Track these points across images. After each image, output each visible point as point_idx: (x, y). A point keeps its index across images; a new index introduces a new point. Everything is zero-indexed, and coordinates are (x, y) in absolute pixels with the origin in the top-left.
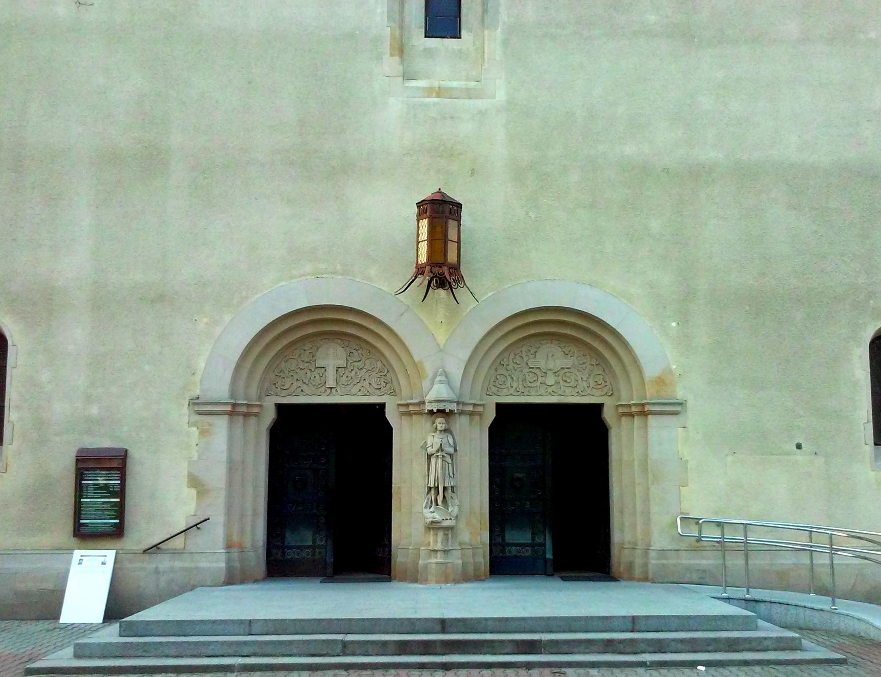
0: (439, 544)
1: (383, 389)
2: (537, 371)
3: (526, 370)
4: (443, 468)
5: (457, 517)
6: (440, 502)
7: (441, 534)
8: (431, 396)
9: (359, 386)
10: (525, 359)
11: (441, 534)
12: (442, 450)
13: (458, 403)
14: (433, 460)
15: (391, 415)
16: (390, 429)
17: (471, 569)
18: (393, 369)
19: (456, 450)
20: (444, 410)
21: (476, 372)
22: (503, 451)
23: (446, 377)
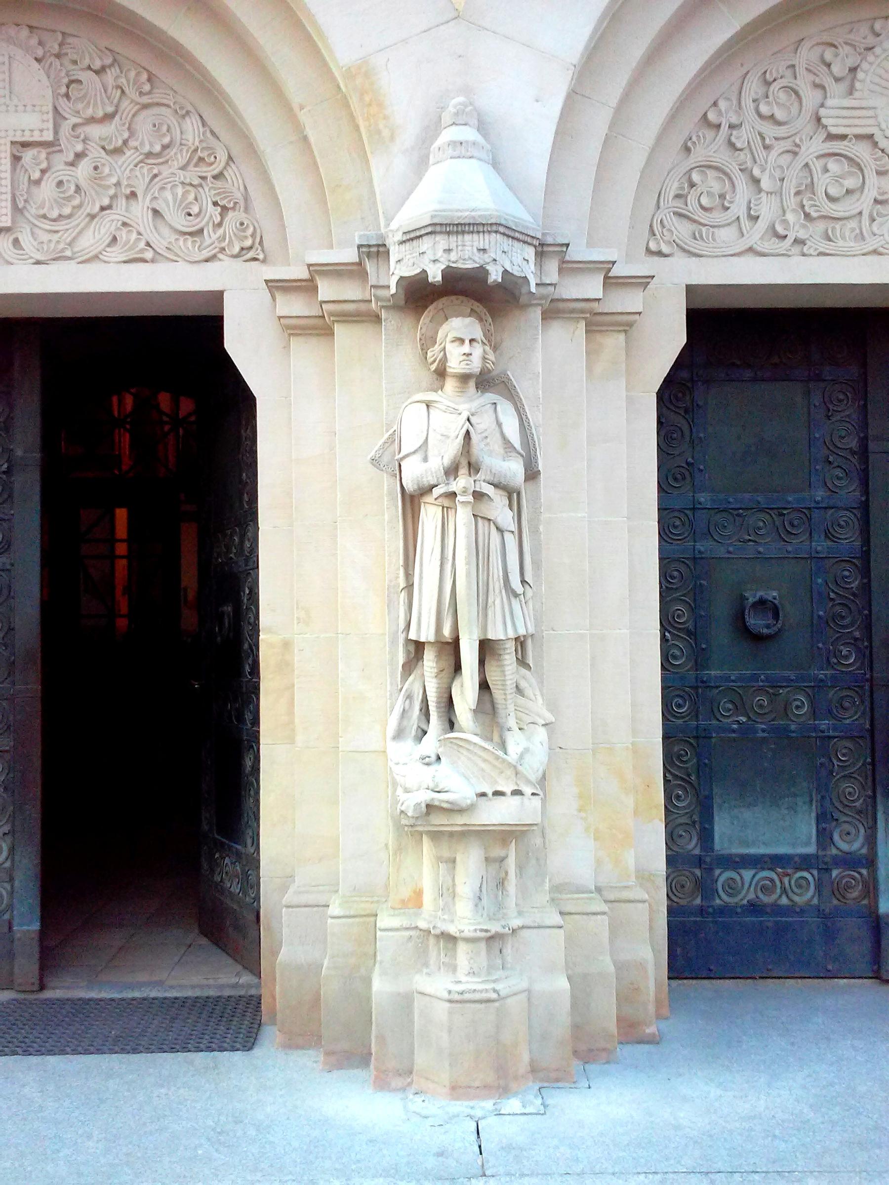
1: (211, 236)
2: (862, 151)
3: (815, 146)
7: (470, 864)
8: (418, 209)
9: (107, 225)
10: (811, 98)
11: (470, 864)
12: (473, 468)
13: (542, 250)
14: (430, 515)
15: (247, 346)
17: (605, 1010)
18: (251, 149)
19: (532, 474)
20: (482, 272)
21: (603, 164)
22: (703, 498)
23: (482, 127)
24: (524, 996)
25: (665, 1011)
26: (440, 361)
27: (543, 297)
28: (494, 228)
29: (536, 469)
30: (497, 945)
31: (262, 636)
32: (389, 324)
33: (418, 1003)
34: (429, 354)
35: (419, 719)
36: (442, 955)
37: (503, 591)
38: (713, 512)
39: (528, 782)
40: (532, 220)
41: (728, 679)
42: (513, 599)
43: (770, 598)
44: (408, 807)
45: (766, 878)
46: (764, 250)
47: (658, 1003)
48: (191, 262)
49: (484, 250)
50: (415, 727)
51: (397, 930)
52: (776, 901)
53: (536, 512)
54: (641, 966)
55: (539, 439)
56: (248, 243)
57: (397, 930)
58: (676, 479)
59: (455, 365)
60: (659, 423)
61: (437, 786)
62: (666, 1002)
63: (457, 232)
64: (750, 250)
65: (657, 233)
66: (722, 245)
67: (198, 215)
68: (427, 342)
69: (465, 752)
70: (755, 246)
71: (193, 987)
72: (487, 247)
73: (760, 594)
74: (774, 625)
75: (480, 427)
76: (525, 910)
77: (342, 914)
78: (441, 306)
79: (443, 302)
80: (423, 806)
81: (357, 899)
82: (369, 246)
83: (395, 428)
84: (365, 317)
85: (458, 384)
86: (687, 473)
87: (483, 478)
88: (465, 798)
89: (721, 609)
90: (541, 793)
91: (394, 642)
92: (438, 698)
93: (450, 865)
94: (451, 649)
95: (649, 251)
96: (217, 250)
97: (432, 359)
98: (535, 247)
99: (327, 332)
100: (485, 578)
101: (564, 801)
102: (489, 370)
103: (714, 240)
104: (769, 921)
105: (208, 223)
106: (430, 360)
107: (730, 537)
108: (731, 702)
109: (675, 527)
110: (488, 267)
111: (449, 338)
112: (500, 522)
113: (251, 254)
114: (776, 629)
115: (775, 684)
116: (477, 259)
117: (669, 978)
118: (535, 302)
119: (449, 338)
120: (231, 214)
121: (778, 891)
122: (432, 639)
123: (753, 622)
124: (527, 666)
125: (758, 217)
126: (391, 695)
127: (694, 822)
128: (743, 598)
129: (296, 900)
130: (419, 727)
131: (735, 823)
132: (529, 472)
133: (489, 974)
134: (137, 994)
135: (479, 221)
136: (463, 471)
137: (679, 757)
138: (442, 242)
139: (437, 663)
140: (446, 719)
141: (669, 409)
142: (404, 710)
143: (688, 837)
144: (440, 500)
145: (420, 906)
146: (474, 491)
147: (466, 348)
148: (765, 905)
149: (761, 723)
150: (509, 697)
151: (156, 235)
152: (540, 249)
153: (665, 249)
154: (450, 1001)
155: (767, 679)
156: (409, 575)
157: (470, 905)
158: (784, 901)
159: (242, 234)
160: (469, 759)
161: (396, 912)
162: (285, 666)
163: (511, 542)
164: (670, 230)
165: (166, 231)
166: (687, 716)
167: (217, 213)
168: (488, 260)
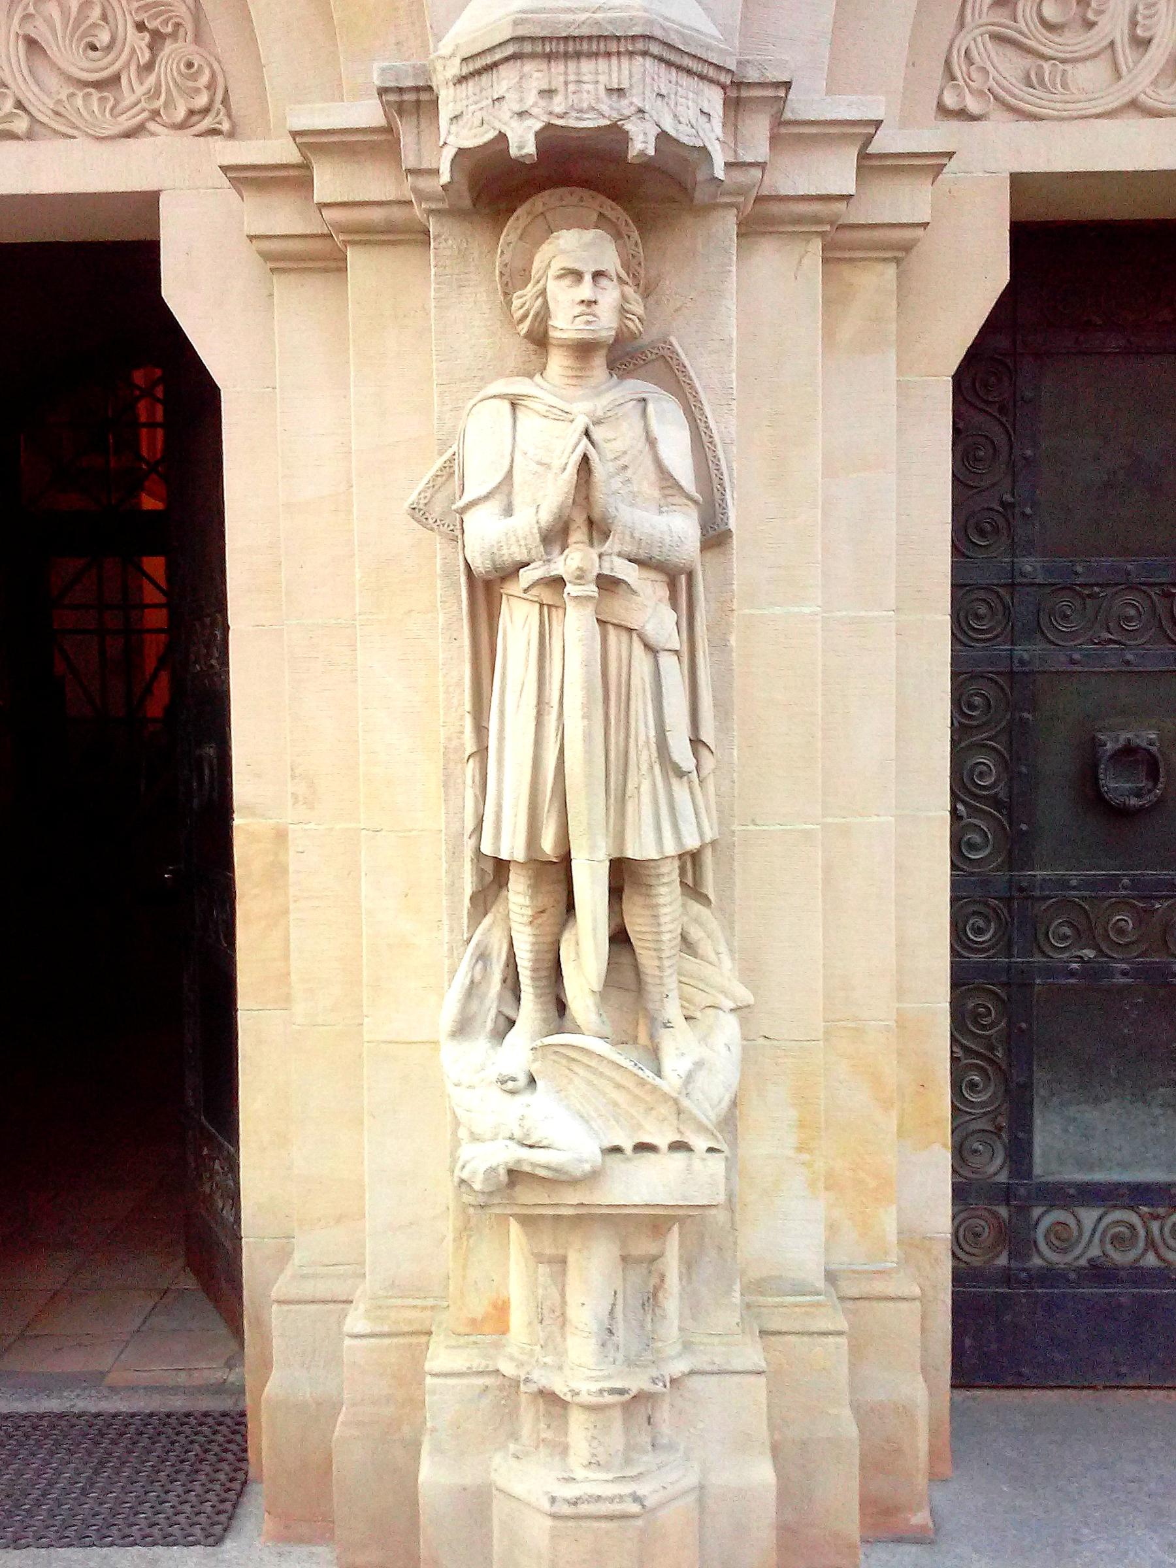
0: (581, 1349)
1: (133, 90)
4: (610, 692)
5: (730, 1122)
6: (127, 50)
11: (593, 1273)
13: (739, 97)
14: (518, 619)
15: (204, 293)
16: (192, 402)
17: (840, 1497)
19: (715, 538)
20: (616, 133)
22: (1029, 565)
24: (691, 1498)
25: (946, 1469)
26: (537, 314)
27: (741, 191)
28: (640, 46)
29: (723, 528)
30: (642, 1412)
31: (238, 821)
32: (443, 245)
33: (499, 1510)
34: (516, 303)
35: (500, 997)
36: (542, 1426)
37: (657, 768)
38: (1048, 590)
39: (701, 1128)
40: (717, 33)
41: (1064, 884)
42: (674, 781)
43: (1144, 744)
44: (474, 1173)
45: (1118, 1223)
46: (1163, 106)
47: (933, 1454)
48: (97, 138)
49: (620, 91)
50: (493, 1012)
51: (460, 1375)
52: (1137, 1260)
53: (724, 610)
54: (905, 1411)
55: (730, 468)
56: (202, 101)
57: (460, 1375)
58: (982, 533)
59: (565, 324)
60: (956, 430)
61: (527, 1135)
62: (947, 1454)
63: (566, 55)
64: (1134, 105)
65: (958, 75)
66: (1083, 97)
67: (109, 47)
68: (515, 278)
69: (582, 1072)
70: (1143, 97)
71: (149, 1389)
72: (625, 85)
73: (1124, 736)
74: (1150, 791)
75: (610, 450)
76: (697, 1340)
77: (368, 1331)
78: (539, 207)
79: (539, 202)
80: (502, 1171)
81: (399, 1302)
82: (400, 90)
83: (455, 448)
84: (400, 234)
85: (568, 362)
86: (1001, 523)
87: (617, 548)
88: (581, 1161)
89: (1056, 761)
90: (727, 1153)
91: (455, 854)
92: (536, 961)
93: (557, 1267)
94: (557, 873)
95: (943, 111)
96: (145, 115)
97: (521, 311)
98: (724, 87)
99: (335, 265)
100: (622, 744)
101: (769, 1140)
102: (632, 333)
103: (1064, 85)
104: (1125, 1293)
105: (127, 64)
106: (518, 315)
107: (1073, 635)
108: (1071, 925)
109: (978, 618)
110: (628, 126)
111: (552, 272)
112: (651, 631)
113: (207, 123)
114: (1151, 797)
115: (1146, 891)
116: (604, 108)
117: (953, 1386)
118: (726, 200)
119: (552, 272)
120: (169, 47)
121: (1141, 1244)
122: (520, 855)
123: (1112, 785)
124: (704, 899)
125: (1149, 41)
126: (451, 949)
127: (1000, 1128)
128: (1095, 745)
129: (293, 1292)
130: (500, 1012)
131: (1071, 1129)
132: (711, 532)
133: (628, 1462)
134: (52, 1404)
135: (609, 30)
136: (578, 535)
137: (976, 1017)
138: (536, 75)
139: (531, 897)
140: (551, 998)
141: (971, 404)
142: (472, 982)
143: (987, 1156)
144: (534, 591)
145: (505, 1331)
146: (599, 576)
147: (586, 290)
148: (1117, 1268)
149: (1123, 961)
150: (666, 963)
151: (36, 89)
152: (733, 94)
153: (973, 106)
154: (554, 1516)
155: (1136, 883)
156: (480, 730)
157: (592, 1345)
158: (1151, 1260)
159: (190, 84)
160: (590, 1083)
161: (462, 1340)
162: (277, 872)
163: (673, 671)
164: (983, 70)
165: (53, 81)
166: (992, 947)
167: (143, 44)
168: (627, 112)
